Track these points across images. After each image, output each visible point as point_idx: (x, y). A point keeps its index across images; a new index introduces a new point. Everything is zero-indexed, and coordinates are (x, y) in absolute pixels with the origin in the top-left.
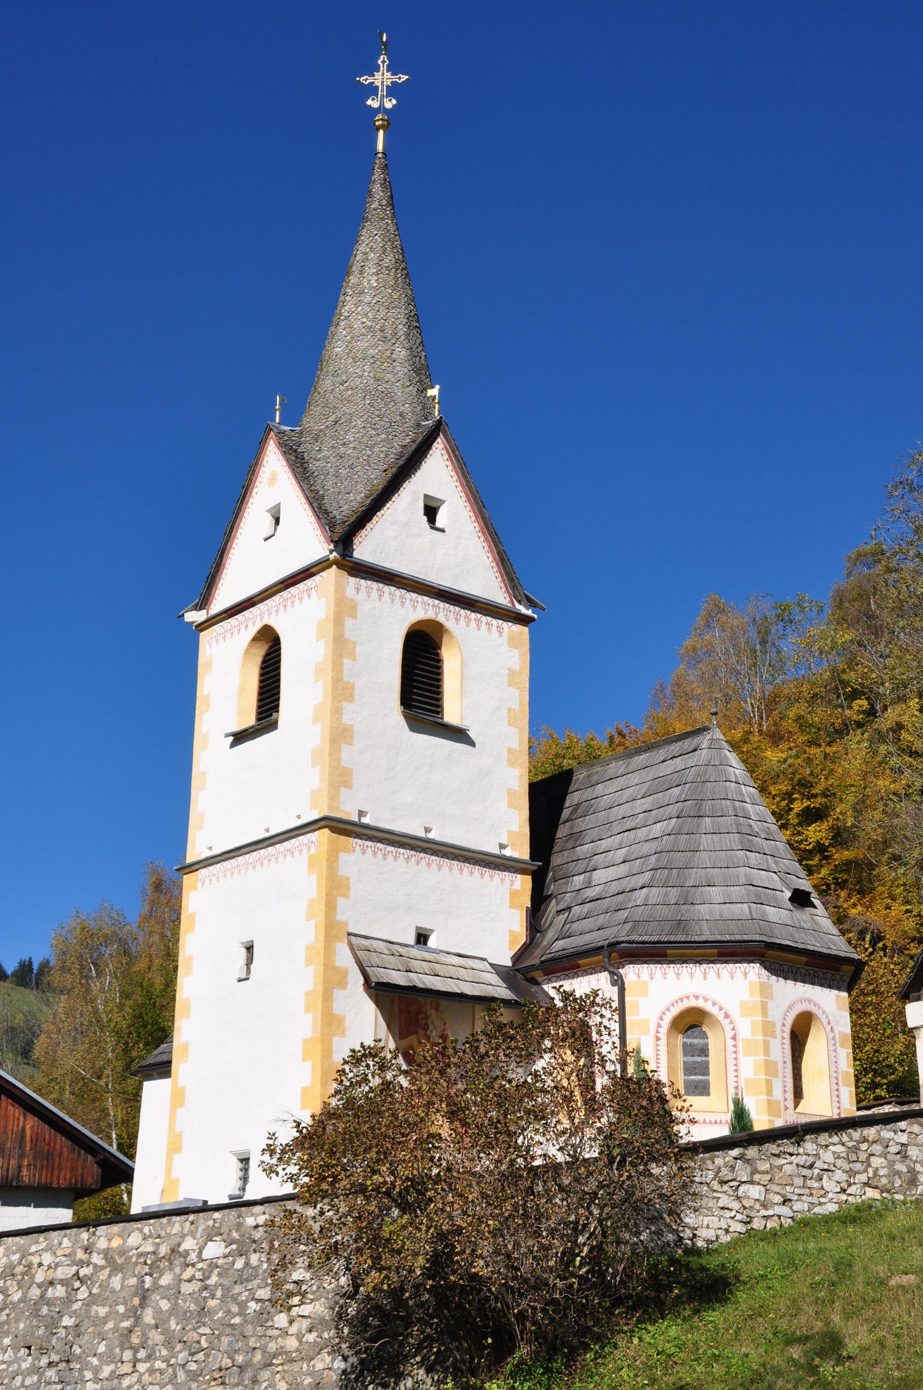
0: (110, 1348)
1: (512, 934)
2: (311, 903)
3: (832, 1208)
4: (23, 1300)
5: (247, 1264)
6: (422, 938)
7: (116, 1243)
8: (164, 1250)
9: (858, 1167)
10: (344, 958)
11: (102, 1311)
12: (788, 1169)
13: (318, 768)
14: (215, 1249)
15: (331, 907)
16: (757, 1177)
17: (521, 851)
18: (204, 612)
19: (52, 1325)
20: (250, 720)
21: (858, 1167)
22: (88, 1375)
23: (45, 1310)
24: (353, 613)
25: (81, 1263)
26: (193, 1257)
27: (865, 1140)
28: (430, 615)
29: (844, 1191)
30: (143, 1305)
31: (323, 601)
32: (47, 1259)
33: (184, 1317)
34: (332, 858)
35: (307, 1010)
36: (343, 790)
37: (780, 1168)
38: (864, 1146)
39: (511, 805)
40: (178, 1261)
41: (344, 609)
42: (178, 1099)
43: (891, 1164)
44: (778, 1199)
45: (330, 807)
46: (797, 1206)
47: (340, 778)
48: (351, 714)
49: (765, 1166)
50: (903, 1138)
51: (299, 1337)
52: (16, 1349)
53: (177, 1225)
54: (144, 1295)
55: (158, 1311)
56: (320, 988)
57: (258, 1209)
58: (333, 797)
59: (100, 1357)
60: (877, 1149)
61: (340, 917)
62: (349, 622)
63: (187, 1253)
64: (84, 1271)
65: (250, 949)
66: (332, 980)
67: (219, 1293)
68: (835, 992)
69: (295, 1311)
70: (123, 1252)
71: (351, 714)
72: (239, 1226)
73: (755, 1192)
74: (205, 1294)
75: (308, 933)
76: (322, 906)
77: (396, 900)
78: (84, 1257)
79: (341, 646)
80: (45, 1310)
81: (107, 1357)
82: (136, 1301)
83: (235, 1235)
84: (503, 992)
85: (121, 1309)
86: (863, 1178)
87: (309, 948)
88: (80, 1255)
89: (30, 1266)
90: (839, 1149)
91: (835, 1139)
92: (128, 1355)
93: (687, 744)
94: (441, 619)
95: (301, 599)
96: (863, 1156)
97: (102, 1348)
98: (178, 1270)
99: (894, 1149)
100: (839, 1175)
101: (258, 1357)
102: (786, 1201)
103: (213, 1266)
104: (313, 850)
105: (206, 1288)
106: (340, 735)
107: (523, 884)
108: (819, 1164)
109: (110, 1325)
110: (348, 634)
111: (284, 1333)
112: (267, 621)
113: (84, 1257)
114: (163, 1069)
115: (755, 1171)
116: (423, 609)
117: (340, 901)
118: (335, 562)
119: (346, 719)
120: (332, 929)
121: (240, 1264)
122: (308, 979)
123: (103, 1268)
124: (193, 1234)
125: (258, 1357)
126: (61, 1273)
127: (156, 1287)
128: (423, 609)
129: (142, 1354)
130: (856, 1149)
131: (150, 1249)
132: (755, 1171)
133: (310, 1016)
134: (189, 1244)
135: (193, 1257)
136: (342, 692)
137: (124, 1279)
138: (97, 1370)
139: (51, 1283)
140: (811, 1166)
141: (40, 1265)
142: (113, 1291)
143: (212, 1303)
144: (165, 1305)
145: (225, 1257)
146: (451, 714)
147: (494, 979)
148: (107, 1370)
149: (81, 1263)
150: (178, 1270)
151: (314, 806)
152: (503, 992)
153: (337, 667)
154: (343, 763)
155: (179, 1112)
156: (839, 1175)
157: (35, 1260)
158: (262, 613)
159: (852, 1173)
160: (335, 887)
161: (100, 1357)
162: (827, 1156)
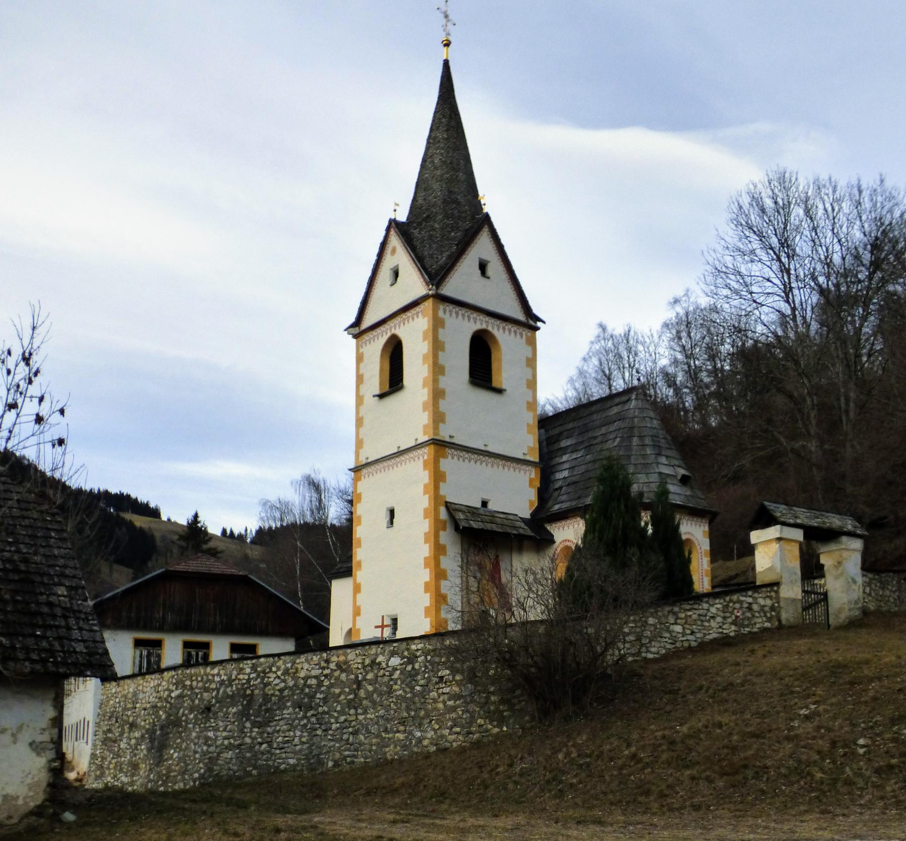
0: (343, 709)
1: (531, 503)
2: (425, 486)
3: (715, 635)
4: (295, 685)
5: (413, 668)
6: (484, 504)
7: (342, 658)
8: (367, 662)
9: (728, 615)
10: (443, 514)
11: (337, 691)
12: (695, 617)
13: (426, 413)
14: (395, 661)
15: (437, 488)
16: (679, 621)
17: (535, 458)
18: (357, 328)
19: (312, 697)
20: (387, 388)
21: (728, 615)
22: (333, 720)
23: (307, 690)
24: (443, 326)
25: (324, 668)
26: (384, 665)
27: (731, 601)
28: (484, 326)
29: (720, 627)
30: (359, 688)
31: (426, 319)
32: (306, 666)
33: (381, 694)
34: (436, 462)
35: (426, 542)
36: (441, 425)
37: (690, 616)
38: (731, 604)
39: (529, 432)
40: (375, 667)
41: (437, 324)
42: (357, 589)
43: (743, 614)
44: (688, 632)
45: (435, 434)
46: (699, 635)
47: (438, 418)
48: (443, 382)
49: (682, 615)
50: (750, 600)
51: (444, 702)
52: (294, 708)
53: (373, 650)
54: (359, 684)
55: (367, 691)
56: (433, 530)
57: (416, 641)
58: (436, 428)
59: (338, 712)
60: (737, 606)
61: (442, 492)
62: (441, 331)
63: (380, 663)
64: (327, 672)
65: (392, 512)
66: (438, 526)
67: (399, 682)
68: (773, 528)
69: (440, 691)
70: (346, 662)
71: (443, 382)
72: (408, 649)
73: (678, 628)
74: (391, 683)
75: (425, 502)
76: (432, 487)
77: (472, 485)
78: (325, 665)
79: (437, 346)
80: (307, 690)
81: (342, 713)
82: (355, 686)
83: (406, 653)
84: (529, 533)
85: (347, 690)
86: (730, 620)
87: (425, 510)
88: (323, 664)
89: (297, 669)
90: (719, 606)
91: (717, 601)
92: (352, 711)
93: (624, 398)
94: (490, 328)
95: (413, 319)
96: (730, 610)
97: (339, 708)
98: (376, 671)
99: (745, 605)
100: (719, 619)
101: (422, 713)
102: (692, 633)
103: (395, 669)
104: (426, 457)
105: (392, 680)
106: (438, 394)
107: (533, 474)
108: (709, 614)
109: (342, 697)
110: (441, 337)
111: (435, 701)
112: (393, 331)
113: (325, 665)
114: (347, 572)
115: (677, 618)
116: (479, 323)
117: (441, 484)
118: (433, 296)
119: (441, 385)
120: (437, 499)
121: (409, 668)
122: (425, 526)
123: (335, 670)
124: (383, 654)
125: (422, 713)
126: (314, 673)
127: (365, 679)
128: (479, 323)
129: (360, 711)
130: (727, 606)
131: (360, 661)
132: (677, 618)
133: (427, 545)
134: (380, 659)
135: (384, 665)
136: (438, 370)
137: (347, 676)
138: (337, 719)
139: (309, 677)
140: (706, 615)
141: (302, 668)
142: (342, 681)
143: (395, 687)
144: (370, 688)
145: (401, 665)
146: (495, 384)
147: (523, 525)
148: (342, 718)
149: (324, 668)
150: (376, 671)
151: (425, 434)
152: (529, 533)
153: (435, 356)
154: (441, 409)
155: (358, 595)
156: (719, 619)
157: (299, 666)
158: (391, 328)
159: (725, 618)
160: (438, 477)
161: (338, 712)
162: (713, 610)
